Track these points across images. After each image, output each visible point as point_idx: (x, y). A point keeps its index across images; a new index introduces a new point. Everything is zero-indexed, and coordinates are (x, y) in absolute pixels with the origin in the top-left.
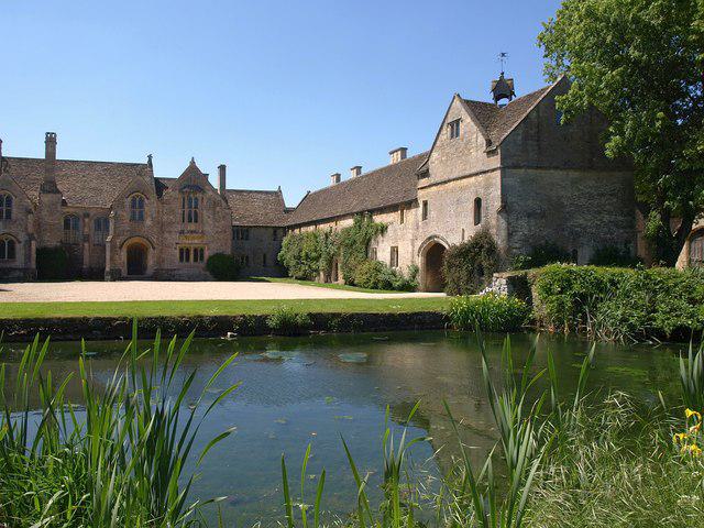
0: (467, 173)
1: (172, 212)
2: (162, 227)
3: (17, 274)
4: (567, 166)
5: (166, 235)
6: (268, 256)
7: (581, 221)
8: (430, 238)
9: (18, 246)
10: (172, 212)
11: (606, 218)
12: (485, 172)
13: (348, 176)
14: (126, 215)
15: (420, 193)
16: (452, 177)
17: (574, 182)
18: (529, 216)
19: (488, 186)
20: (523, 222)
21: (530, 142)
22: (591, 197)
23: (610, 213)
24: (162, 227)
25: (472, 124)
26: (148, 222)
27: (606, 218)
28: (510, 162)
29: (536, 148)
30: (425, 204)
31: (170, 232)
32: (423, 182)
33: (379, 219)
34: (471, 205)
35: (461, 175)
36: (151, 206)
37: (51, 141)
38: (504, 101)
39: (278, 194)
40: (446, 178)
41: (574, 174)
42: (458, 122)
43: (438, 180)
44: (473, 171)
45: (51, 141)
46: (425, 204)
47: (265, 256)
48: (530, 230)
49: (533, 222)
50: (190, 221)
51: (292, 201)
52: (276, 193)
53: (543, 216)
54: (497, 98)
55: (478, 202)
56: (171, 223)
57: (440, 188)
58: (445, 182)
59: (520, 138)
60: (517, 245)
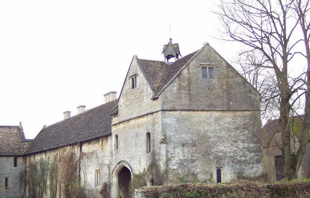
0: (142, 114)
4: (210, 108)
6: (9, 181)
7: (222, 148)
8: (120, 162)
11: (241, 145)
12: (152, 113)
13: (75, 113)
15: (114, 129)
16: (132, 117)
17: (217, 119)
18: (183, 145)
19: (154, 124)
20: (179, 150)
21: (182, 91)
22: (229, 130)
23: (243, 141)
25: (144, 78)
27: (241, 145)
29: (187, 96)
30: (117, 137)
32: (115, 120)
33: (86, 148)
34: (144, 138)
35: (138, 115)
36: (257, 112)
38: (173, 60)
39: (19, 129)
40: (128, 118)
41: (217, 114)
42: (136, 75)
43: (124, 119)
44: (146, 113)
46: (117, 137)
47: (6, 180)
49: (186, 150)
51: (31, 134)
53: (194, 145)
54: (168, 57)
55: (149, 134)
57: (126, 125)
58: (128, 120)
59: (175, 88)
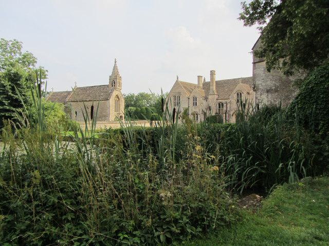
9: (199, 116)
18: (268, 91)
37: (212, 73)
45: (212, 73)
49: (270, 96)
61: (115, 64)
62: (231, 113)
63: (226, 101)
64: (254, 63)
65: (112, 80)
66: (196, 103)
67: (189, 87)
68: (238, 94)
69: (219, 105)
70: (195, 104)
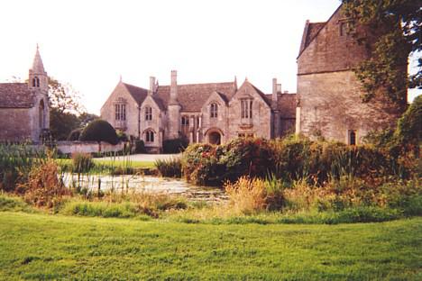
1: (234, 112)
2: (228, 121)
3: (154, 150)
5: (230, 127)
7: (358, 110)
9: (155, 135)
10: (234, 112)
14: (207, 115)
20: (311, 113)
24: (228, 121)
26: (220, 118)
28: (303, 71)
31: (232, 125)
37: (174, 74)
45: (174, 74)
48: (317, 119)
49: (318, 112)
50: (243, 117)
52: (232, 83)
53: (327, 107)
56: (233, 119)
60: (307, 130)
61: (38, 52)
62: (204, 132)
63: (193, 114)
64: (298, 75)
65: (33, 77)
66: (151, 116)
67: (139, 94)
68: (212, 106)
69: (183, 119)
70: (149, 117)
